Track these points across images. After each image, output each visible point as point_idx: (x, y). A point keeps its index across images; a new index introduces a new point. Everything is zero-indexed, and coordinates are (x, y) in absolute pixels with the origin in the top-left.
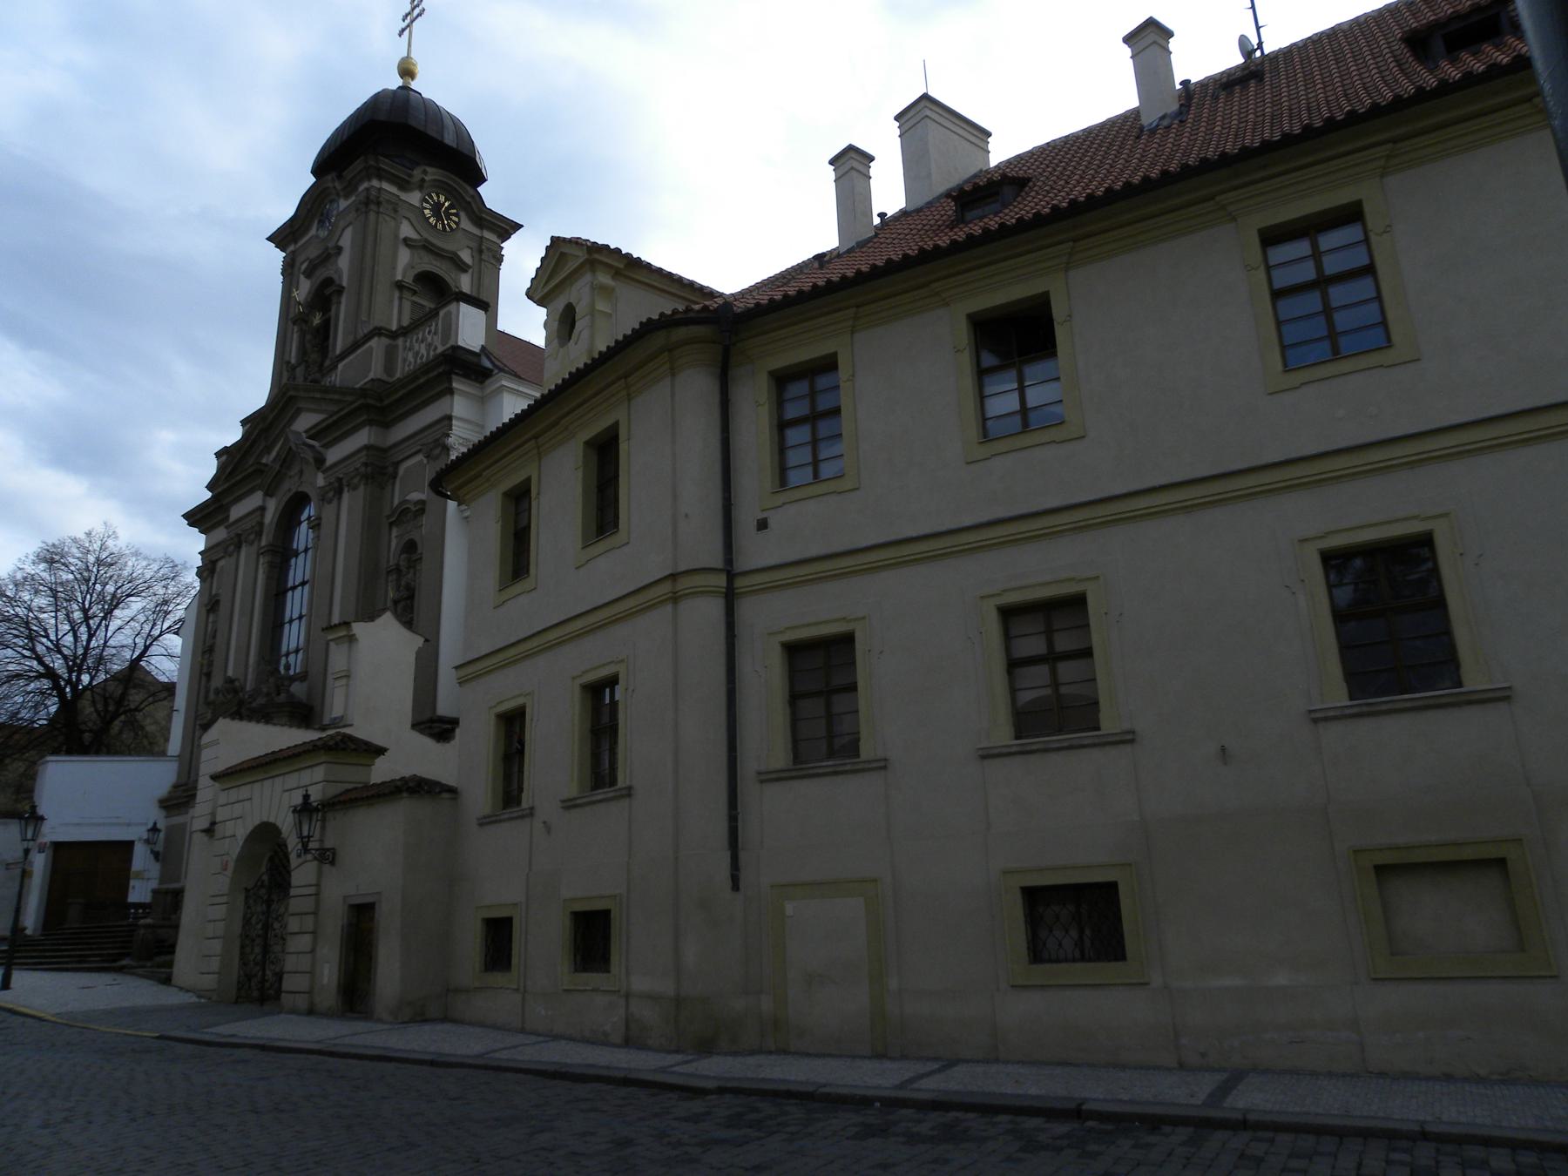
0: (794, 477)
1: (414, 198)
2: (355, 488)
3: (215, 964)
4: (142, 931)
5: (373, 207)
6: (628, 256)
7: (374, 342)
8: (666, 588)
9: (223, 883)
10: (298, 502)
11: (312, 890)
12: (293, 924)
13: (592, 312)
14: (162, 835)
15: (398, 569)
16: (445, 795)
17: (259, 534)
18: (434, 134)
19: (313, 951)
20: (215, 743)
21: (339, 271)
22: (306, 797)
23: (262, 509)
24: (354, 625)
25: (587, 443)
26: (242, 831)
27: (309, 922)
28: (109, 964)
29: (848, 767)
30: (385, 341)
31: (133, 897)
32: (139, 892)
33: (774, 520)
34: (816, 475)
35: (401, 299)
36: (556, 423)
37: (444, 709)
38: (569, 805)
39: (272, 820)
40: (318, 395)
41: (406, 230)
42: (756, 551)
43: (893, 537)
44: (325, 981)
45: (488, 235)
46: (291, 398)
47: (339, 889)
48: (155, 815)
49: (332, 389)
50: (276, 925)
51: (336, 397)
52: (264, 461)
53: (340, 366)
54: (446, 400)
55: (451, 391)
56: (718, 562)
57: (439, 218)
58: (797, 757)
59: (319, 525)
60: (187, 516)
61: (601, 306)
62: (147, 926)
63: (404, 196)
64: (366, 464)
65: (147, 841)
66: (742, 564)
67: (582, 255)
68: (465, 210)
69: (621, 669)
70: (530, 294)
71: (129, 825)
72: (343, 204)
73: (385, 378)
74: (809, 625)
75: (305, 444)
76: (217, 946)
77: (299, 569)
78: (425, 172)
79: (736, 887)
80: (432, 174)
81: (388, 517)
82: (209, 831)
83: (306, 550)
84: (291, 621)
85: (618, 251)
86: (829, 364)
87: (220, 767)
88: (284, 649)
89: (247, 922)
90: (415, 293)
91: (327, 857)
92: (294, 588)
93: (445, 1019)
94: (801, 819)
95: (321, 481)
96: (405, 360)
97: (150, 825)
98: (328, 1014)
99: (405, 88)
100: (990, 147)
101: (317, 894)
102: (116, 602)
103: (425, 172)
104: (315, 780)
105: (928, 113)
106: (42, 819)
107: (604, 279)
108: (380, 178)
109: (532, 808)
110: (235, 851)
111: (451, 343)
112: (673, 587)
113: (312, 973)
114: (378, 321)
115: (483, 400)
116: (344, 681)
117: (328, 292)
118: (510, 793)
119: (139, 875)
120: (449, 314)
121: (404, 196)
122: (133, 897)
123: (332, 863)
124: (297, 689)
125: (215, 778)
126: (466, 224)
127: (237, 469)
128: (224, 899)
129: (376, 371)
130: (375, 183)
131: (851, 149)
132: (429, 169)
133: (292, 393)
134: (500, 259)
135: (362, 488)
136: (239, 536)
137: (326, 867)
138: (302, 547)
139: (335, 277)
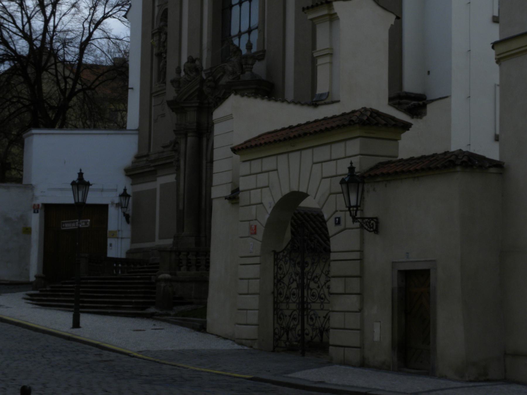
3: (253, 317)
4: (163, 284)
8: (326, 320)
9: (254, 245)
12: (337, 286)
14: (131, 199)
16: (493, 170)
19: (361, 310)
20: (229, 117)
22: (351, 169)
24: (335, 4)
26: (270, 200)
27: (355, 285)
28: (138, 311)
31: (112, 253)
32: (117, 249)
37: (410, 86)
39: (295, 189)
47: (384, 257)
48: (123, 183)
50: (312, 285)
62: (166, 280)
65: (118, 205)
71: (102, 190)
76: (253, 301)
82: (234, 197)
87: (238, 141)
88: (234, 31)
89: (278, 281)
91: (372, 225)
93: (506, 380)
97: (121, 191)
98: (382, 367)
101: (361, 260)
104: (351, 152)
106: (88, 184)
113: (361, 330)
116: (327, 59)
119: (114, 235)
122: (112, 253)
123: (376, 231)
124: (259, 68)
125: (235, 150)
128: (257, 260)
137: (369, 235)
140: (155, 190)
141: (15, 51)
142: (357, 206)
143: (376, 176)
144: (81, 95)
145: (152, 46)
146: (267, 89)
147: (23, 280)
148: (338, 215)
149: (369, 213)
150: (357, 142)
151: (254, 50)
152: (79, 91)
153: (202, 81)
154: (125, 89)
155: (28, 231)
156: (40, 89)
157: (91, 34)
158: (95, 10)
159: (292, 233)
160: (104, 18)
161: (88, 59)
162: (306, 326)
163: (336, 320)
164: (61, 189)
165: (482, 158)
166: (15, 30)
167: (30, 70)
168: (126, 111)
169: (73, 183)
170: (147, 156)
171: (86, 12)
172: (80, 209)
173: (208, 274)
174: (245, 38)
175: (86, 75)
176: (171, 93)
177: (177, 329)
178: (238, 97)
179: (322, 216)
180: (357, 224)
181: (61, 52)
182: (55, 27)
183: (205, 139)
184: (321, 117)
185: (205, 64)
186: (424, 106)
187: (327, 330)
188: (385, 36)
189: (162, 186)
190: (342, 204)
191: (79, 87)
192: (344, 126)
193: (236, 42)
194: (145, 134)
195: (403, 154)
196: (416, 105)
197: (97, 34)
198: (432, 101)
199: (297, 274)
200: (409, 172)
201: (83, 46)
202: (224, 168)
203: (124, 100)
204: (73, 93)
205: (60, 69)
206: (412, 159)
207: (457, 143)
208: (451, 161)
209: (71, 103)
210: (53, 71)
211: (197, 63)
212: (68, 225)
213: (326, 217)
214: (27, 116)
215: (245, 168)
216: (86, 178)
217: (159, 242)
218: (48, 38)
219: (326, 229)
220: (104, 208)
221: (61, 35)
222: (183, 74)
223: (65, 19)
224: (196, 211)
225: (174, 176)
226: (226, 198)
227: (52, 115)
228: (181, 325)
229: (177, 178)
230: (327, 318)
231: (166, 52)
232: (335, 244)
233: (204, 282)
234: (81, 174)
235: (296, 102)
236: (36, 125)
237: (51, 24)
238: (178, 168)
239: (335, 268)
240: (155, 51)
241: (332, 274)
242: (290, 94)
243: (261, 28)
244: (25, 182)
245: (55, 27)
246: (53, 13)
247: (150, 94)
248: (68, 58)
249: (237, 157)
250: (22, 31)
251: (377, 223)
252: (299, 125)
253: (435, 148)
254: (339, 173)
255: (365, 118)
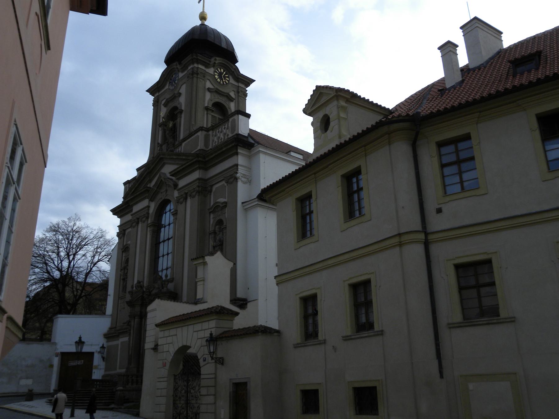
0: (449, 190)
1: (211, 71)
2: (194, 197)
4: (119, 393)
5: (195, 75)
6: (352, 93)
7: (199, 133)
8: (397, 240)
9: (164, 372)
10: (166, 202)
11: (213, 376)
12: (204, 391)
13: (339, 118)
15: (215, 233)
16: (275, 334)
17: (148, 218)
18: (218, 44)
21: (180, 104)
22: (211, 334)
23: (148, 207)
24: (206, 258)
25: (343, 176)
26: (173, 350)
27: (212, 390)
29: (495, 321)
30: (204, 133)
32: (97, 375)
33: (445, 208)
34: (463, 188)
35: (207, 114)
36: (327, 167)
37: (240, 294)
38: (346, 338)
39: (185, 344)
40: (175, 157)
41: (208, 85)
42: (437, 223)
43: (507, 216)
44: (222, 417)
45: (241, 85)
46: (162, 159)
47: (226, 376)
48: (102, 341)
49: (179, 154)
50: (192, 391)
51: (184, 157)
52: (148, 186)
53: (183, 144)
54: (235, 157)
55: (237, 154)
56: (420, 228)
57: (221, 79)
58: (465, 317)
59: (176, 213)
60: (112, 211)
61: (342, 115)
62: (121, 390)
63: (207, 70)
64: (199, 187)
65: (99, 352)
66: (430, 229)
67: (333, 94)
68: (231, 75)
69: (372, 277)
70: (305, 111)
71: (92, 345)
72: (181, 75)
73: (204, 148)
74: (467, 256)
75: (169, 178)
76: (163, 400)
77: (164, 233)
78: (216, 60)
79: (442, 376)
80: (219, 60)
81: (209, 209)
82: (156, 348)
83: (169, 225)
84: (163, 256)
85: (348, 91)
86: (467, 137)
87: (158, 321)
88: (160, 269)
89: (176, 389)
90: (213, 111)
91: (220, 361)
92: (164, 241)
94: (469, 344)
95: (176, 194)
96: (213, 141)
97: (101, 345)
99: (202, 25)
100: (503, 39)
101: (215, 378)
102: (80, 247)
103: (216, 60)
104: (211, 326)
105: (477, 25)
106: (84, 343)
107: (343, 103)
108: (198, 63)
109: (325, 340)
110: (170, 358)
111: (236, 133)
112: (400, 239)
114: (199, 125)
115: (250, 157)
116: (202, 283)
117: (175, 113)
118: (310, 333)
119: (96, 367)
120: (234, 120)
121: (207, 70)
123: (222, 364)
124: (171, 286)
125: (157, 325)
126: (232, 81)
127: (135, 189)
128: (165, 379)
129: (201, 146)
130: (196, 65)
131: (449, 43)
132: (217, 58)
133: (162, 156)
134: (246, 95)
135: (197, 197)
136: (138, 219)
137: (219, 366)
138: (167, 223)
139: (178, 106)
140: (118, 345)
141: (53, 277)
142: (213, 352)
143: (223, 337)
144: (84, 298)
145: (121, 275)
146: (174, 297)
147: (47, 392)
148: (204, 356)
149: (219, 355)
150: (214, 322)
151: (169, 278)
152: (84, 296)
153: (144, 292)
154: (106, 295)
155: (52, 366)
156: (64, 295)
157: (91, 269)
158: (94, 258)
159: (183, 365)
160: (98, 261)
161: (89, 280)
162: (189, 412)
163: (203, 408)
164: (71, 345)
165: (271, 329)
166: (54, 266)
167: (60, 286)
168: (106, 305)
169: (76, 342)
170: (115, 328)
171: (90, 259)
172: (78, 355)
173: (142, 387)
174: (165, 272)
175: (88, 288)
176: (128, 297)
177: (124, 415)
178: (159, 300)
179: (197, 357)
180: (214, 361)
181: (76, 277)
182: (74, 265)
183: (143, 320)
184: (198, 310)
185: (145, 284)
186: (246, 304)
187: (199, 414)
188: (229, 272)
189: (122, 343)
190: (207, 352)
191: (83, 294)
192: (208, 314)
193: (160, 274)
194: (115, 317)
195: (235, 327)
196: (242, 303)
197: (94, 269)
198: (250, 301)
199: (185, 386)
200: (238, 335)
201: (87, 275)
202: (151, 333)
203: (106, 300)
204: (80, 297)
205: (75, 284)
206: (239, 329)
207: (261, 322)
208: (256, 330)
209: (79, 302)
210: (71, 286)
211: (142, 283)
212: (72, 363)
213: (199, 357)
214: (57, 308)
215: (161, 334)
216: (83, 340)
217: (119, 371)
218: (70, 271)
219: (199, 362)
220: (92, 354)
221: (77, 269)
222: (134, 288)
223: (79, 261)
224: (137, 355)
225: (128, 338)
226: (152, 349)
227: (69, 308)
228: (127, 413)
229: (129, 339)
230: (199, 407)
231: (127, 278)
232: (204, 370)
233: (139, 391)
234: (80, 338)
235: (187, 303)
236: (61, 313)
237: (72, 264)
238: (130, 335)
239: (203, 383)
240: (122, 278)
241: (201, 385)
242: (185, 299)
243: (172, 268)
244: (52, 341)
245: (74, 265)
246: (73, 259)
247: (118, 298)
248: (79, 280)
249: (158, 329)
250: (57, 267)
251: (223, 360)
252: (188, 314)
253: (251, 324)
254: (206, 336)
255: (218, 310)
